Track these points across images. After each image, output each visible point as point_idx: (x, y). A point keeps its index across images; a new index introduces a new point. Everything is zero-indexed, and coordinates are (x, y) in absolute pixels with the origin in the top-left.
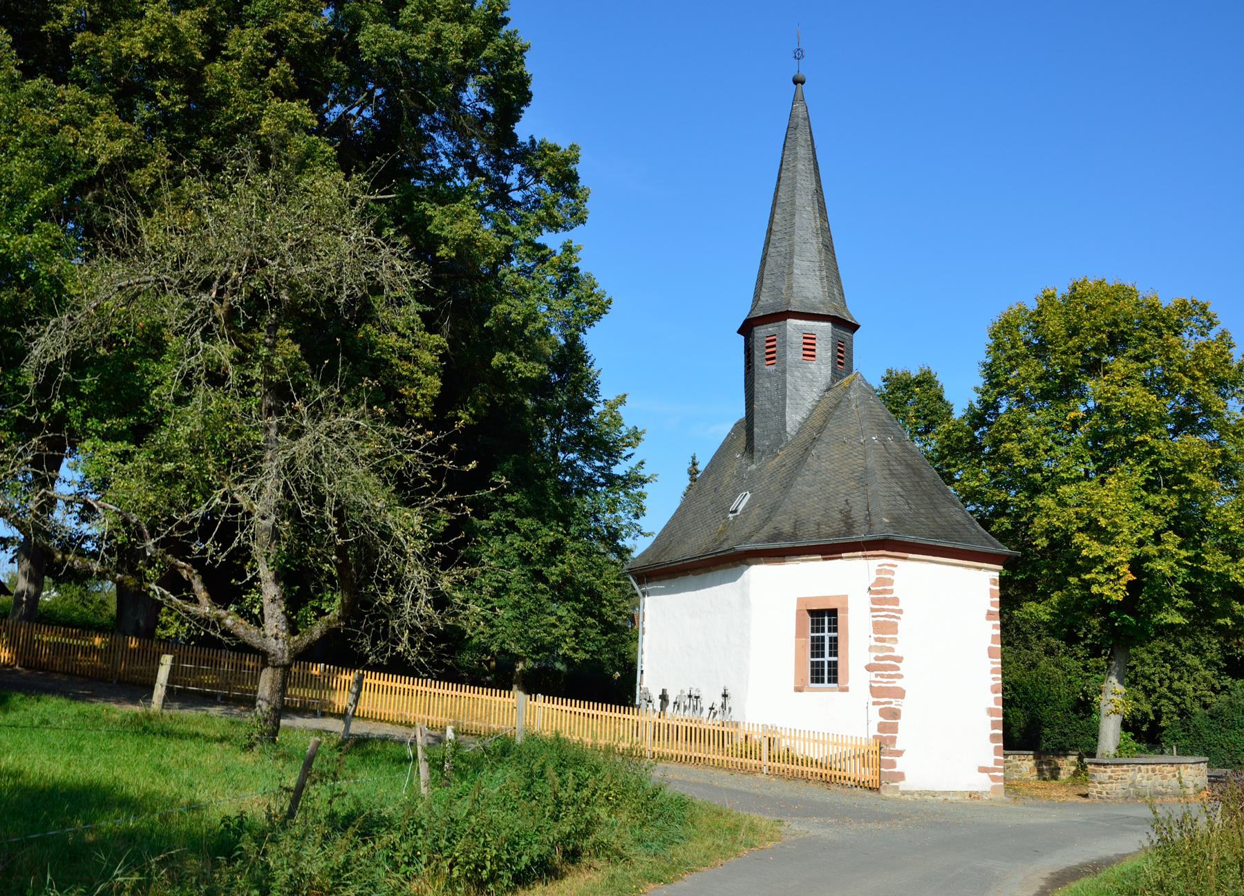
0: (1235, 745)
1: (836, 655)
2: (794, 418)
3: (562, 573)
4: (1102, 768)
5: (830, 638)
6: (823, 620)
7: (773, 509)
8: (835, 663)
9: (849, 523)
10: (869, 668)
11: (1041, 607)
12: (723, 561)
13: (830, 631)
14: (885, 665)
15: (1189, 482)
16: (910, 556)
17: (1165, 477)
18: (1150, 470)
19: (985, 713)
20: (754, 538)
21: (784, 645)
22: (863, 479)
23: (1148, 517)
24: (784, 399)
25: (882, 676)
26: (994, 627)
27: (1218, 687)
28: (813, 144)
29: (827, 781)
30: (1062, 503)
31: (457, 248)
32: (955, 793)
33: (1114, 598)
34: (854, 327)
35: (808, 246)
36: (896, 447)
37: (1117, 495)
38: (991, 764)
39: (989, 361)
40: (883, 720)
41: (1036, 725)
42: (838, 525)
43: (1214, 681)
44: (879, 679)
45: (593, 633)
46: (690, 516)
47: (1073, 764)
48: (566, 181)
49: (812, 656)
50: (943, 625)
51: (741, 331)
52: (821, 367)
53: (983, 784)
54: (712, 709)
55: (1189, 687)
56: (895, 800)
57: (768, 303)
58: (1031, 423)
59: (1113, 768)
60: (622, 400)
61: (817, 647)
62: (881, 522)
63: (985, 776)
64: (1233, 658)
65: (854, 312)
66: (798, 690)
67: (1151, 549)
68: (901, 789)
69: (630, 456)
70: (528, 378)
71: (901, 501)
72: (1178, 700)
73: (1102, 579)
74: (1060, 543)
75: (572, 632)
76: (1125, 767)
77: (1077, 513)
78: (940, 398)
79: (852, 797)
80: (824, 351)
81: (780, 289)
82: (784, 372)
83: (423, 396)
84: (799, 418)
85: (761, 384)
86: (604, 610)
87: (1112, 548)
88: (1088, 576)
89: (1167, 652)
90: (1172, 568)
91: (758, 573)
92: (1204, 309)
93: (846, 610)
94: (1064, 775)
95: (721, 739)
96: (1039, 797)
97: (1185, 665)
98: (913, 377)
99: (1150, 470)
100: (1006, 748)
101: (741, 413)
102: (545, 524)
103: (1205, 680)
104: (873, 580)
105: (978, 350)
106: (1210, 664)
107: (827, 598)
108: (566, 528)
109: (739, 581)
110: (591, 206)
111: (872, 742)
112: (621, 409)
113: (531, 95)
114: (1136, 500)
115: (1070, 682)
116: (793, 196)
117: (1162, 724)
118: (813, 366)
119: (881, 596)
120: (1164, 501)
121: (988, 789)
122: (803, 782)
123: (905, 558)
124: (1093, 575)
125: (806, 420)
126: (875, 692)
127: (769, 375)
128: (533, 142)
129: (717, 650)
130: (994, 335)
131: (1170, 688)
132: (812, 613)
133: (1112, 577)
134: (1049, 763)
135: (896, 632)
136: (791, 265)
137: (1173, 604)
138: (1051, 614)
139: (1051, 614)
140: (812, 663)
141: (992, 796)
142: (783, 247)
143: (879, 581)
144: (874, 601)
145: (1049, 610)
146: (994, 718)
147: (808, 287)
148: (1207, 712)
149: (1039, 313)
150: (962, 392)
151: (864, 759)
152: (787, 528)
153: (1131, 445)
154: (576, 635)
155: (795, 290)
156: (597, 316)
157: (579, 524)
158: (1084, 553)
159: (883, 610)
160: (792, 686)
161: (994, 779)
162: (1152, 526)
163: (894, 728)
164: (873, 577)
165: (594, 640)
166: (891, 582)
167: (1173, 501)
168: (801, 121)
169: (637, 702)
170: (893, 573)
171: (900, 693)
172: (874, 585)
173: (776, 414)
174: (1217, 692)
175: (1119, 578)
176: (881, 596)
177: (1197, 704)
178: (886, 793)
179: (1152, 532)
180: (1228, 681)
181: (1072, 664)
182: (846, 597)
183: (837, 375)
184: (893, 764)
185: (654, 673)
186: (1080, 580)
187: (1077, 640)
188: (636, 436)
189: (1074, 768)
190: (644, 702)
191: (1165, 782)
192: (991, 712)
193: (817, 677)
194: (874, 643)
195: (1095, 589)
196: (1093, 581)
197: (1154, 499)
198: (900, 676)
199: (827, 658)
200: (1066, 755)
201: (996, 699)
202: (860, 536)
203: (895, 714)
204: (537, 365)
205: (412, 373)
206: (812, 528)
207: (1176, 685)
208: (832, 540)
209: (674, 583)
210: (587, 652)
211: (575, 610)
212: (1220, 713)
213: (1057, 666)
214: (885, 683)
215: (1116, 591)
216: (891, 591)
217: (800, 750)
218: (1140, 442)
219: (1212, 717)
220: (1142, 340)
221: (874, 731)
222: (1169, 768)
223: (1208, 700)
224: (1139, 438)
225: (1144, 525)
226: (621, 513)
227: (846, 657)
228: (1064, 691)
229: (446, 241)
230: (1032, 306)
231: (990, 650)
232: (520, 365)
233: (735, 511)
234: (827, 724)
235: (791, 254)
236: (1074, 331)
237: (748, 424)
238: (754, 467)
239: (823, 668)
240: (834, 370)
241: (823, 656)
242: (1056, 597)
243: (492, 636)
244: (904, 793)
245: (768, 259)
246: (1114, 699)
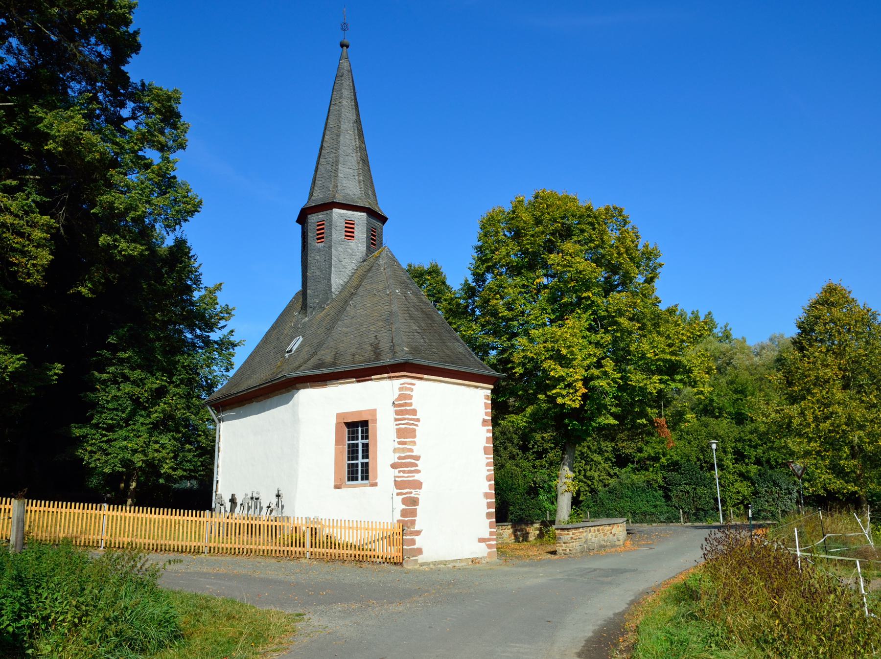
0: (623, 508)
1: (367, 457)
2: (337, 281)
3: (164, 411)
4: (566, 532)
5: (363, 444)
6: (356, 430)
7: (320, 345)
8: (367, 464)
9: (377, 352)
10: (394, 466)
11: (519, 417)
12: (276, 389)
13: (362, 439)
14: (406, 463)
15: (616, 323)
16: (425, 376)
17: (601, 322)
18: (592, 317)
19: (482, 496)
20: (302, 368)
22: (389, 320)
23: (592, 350)
24: (330, 267)
25: (404, 472)
26: (488, 431)
27: (612, 473)
28: (354, 89)
29: (359, 561)
30: (531, 340)
31: (65, 143)
32: (461, 560)
33: (573, 406)
34: (383, 219)
35: (350, 158)
36: (414, 299)
37: (572, 331)
38: (487, 536)
39: (480, 244)
40: (404, 507)
41: (515, 505)
42: (368, 354)
43: (610, 470)
44: (401, 474)
45: (190, 456)
46: (258, 359)
47: (536, 529)
48: (170, 117)
49: (349, 460)
50: (449, 427)
51: (298, 221)
52: (359, 245)
53: (482, 551)
54: (269, 507)
55: (596, 474)
56: (414, 572)
57: (319, 197)
58: (510, 286)
59: (573, 531)
60: (219, 287)
61: (352, 452)
62: (403, 350)
63: (483, 545)
64: (620, 455)
65: (383, 209)
66: (337, 487)
67: (596, 372)
68: (419, 561)
69: (224, 327)
70: (130, 255)
71: (418, 336)
72: (590, 483)
73: (564, 393)
74: (533, 368)
75: (172, 455)
76: (581, 530)
77: (544, 347)
78: (444, 283)
79: (380, 574)
80: (361, 233)
81: (328, 188)
82: (330, 247)
83: (34, 265)
84: (341, 282)
85: (313, 257)
86: (199, 439)
87: (571, 370)
88: (554, 391)
89: (582, 453)
90: (609, 384)
91: (306, 396)
92: (620, 212)
93: (375, 421)
94: (532, 538)
95: (273, 531)
96: (521, 557)
97: (593, 460)
98: (426, 269)
99: (592, 317)
100: (497, 522)
101: (299, 287)
102: (153, 375)
103: (604, 469)
104: (396, 396)
105: (472, 238)
106: (607, 459)
107: (360, 412)
108: (170, 377)
109: (291, 403)
110: (190, 137)
111: (396, 525)
112: (218, 293)
114: (583, 337)
115: (525, 476)
116: (339, 122)
117: (581, 499)
118: (352, 244)
119: (403, 408)
120: (602, 338)
121: (486, 555)
122: (340, 563)
123: (421, 379)
124: (558, 390)
125: (346, 283)
126: (398, 485)
127: (319, 250)
128: (143, 84)
129: (276, 460)
130: (483, 227)
131: (585, 476)
132: (349, 425)
133: (571, 391)
134: (521, 530)
135: (415, 437)
136: (336, 170)
137: (609, 412)
138: (526, 422)
139: (526, 422)
140: (349, 465)
141: (488, 560)
142: (331, 158)
143: (401, 397)
144: (397, 413)
145: (525, 419)
146: (489, 500)
147: (350, 187)
148: (607, 489)
149: (514, 212)
150: (458, 275)
151: (389, 539)
152: (329, 359)
153: (580, 299)
154: (175, 457)
155: (339, 188)
156: (191, 213)
157: (180, 375)
158: (552, 374)
159: (405, 419)
161: (489, 546)
162: (595, 356)
163: (414, 513)
164: (397, 393)
165: (190, 461)
166: (410, 397)
167: (608, 338)
168: (346, 73)
169: (213, 506)
170: (412, 390)
171: (418, 485)
172: (397, 400)
173: (324, 279)
174: (611, 476)
175: (576, 391)
176: (403, 408)
177: (600, 484)
178: (408, 566)
179: (595, 360)
180: (617, 470)
181: (526, 464)
182: (375, 410)
183: (369, 250)
184: (413, 542)
185: (228, 480)
186: (547, 396)
187: (528, 449)
188: (227, 310)
189: (538, 532)
190: (218, 505)
191: (606, 538)
192: (486, 495)
193: (352, 475)
194: (397, 446)
195: (559, 401)
196: (559, 395)
197: (594, 338)
198: (418, 471)
199: (360, 460)
200: (532, 523)
201: (490, 485)
202: (387, 360)
203: (414, 502)
204: (138, 246)
205: (24, 246)
206: (349, 358)
207: (588, 473)
208: (364, 366)
209: (241, 410)
210: (185, 470)
211: (174, 439)
212: (615, 489)
213: (517, 466)
214: (406, 477)
215: (574, 401)
216: (411, 404)
217: (343, 536)
218: (585, 298)
219: (610, 492)
220: (582, 231)
221: (398, 516)
222: (608, 528)
223: (607, 482)
224: (585, 295)
225: (590, 355)
226: (215, 368)
227: (375, 458)
228: (521, 482)
229: (54, 138)
230: (508, 208)
231: (485, 449)
232: (123, 245)
233: (291, 351)
234: (359, 514)
235: (337, 163)
236: (538, 222)
237: (304, 293)
238: (307, 319)
239: (357, 467)
240: (368, 248)
241: (357, 459)
242: (529, 410)
243: (106, 462)
244: (422, 565)
245: (320, 166)
246: (566, 480)
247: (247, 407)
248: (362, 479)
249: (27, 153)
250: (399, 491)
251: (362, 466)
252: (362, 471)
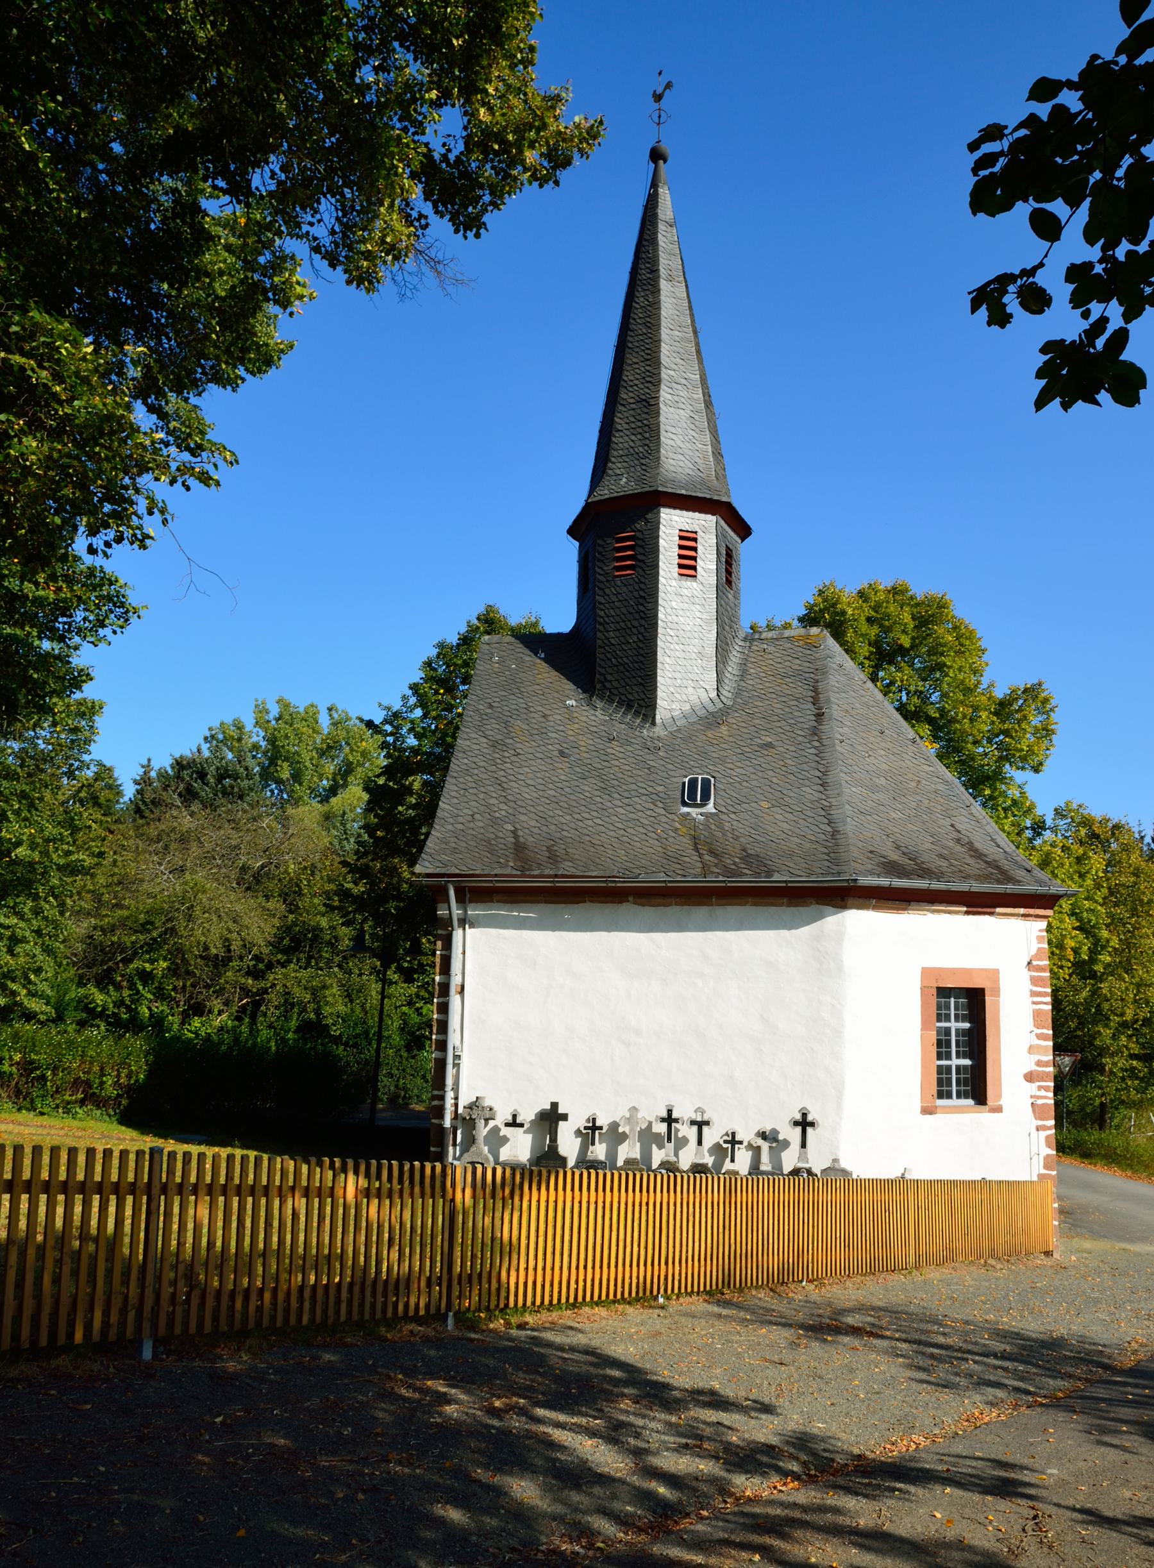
8: (939, 1057)
21: (896, 1042)
91: (858, 924)
93: (996, 992)
109: (806, 931)
113: (1051, 298)
160: (917, 1105)
182: (997, 971)
208: (977, 887)
231: (1037, 1014)
247: (567, 912)
248: (959, 1097)
249: (200, 49)
250: (1040, 1123)
251: (958, 1072)
252: (949, 1084)
